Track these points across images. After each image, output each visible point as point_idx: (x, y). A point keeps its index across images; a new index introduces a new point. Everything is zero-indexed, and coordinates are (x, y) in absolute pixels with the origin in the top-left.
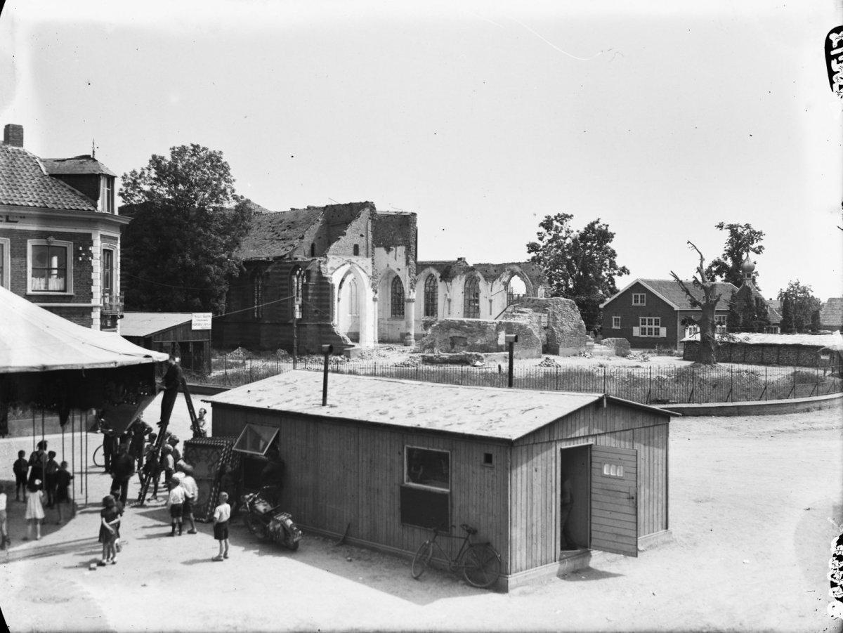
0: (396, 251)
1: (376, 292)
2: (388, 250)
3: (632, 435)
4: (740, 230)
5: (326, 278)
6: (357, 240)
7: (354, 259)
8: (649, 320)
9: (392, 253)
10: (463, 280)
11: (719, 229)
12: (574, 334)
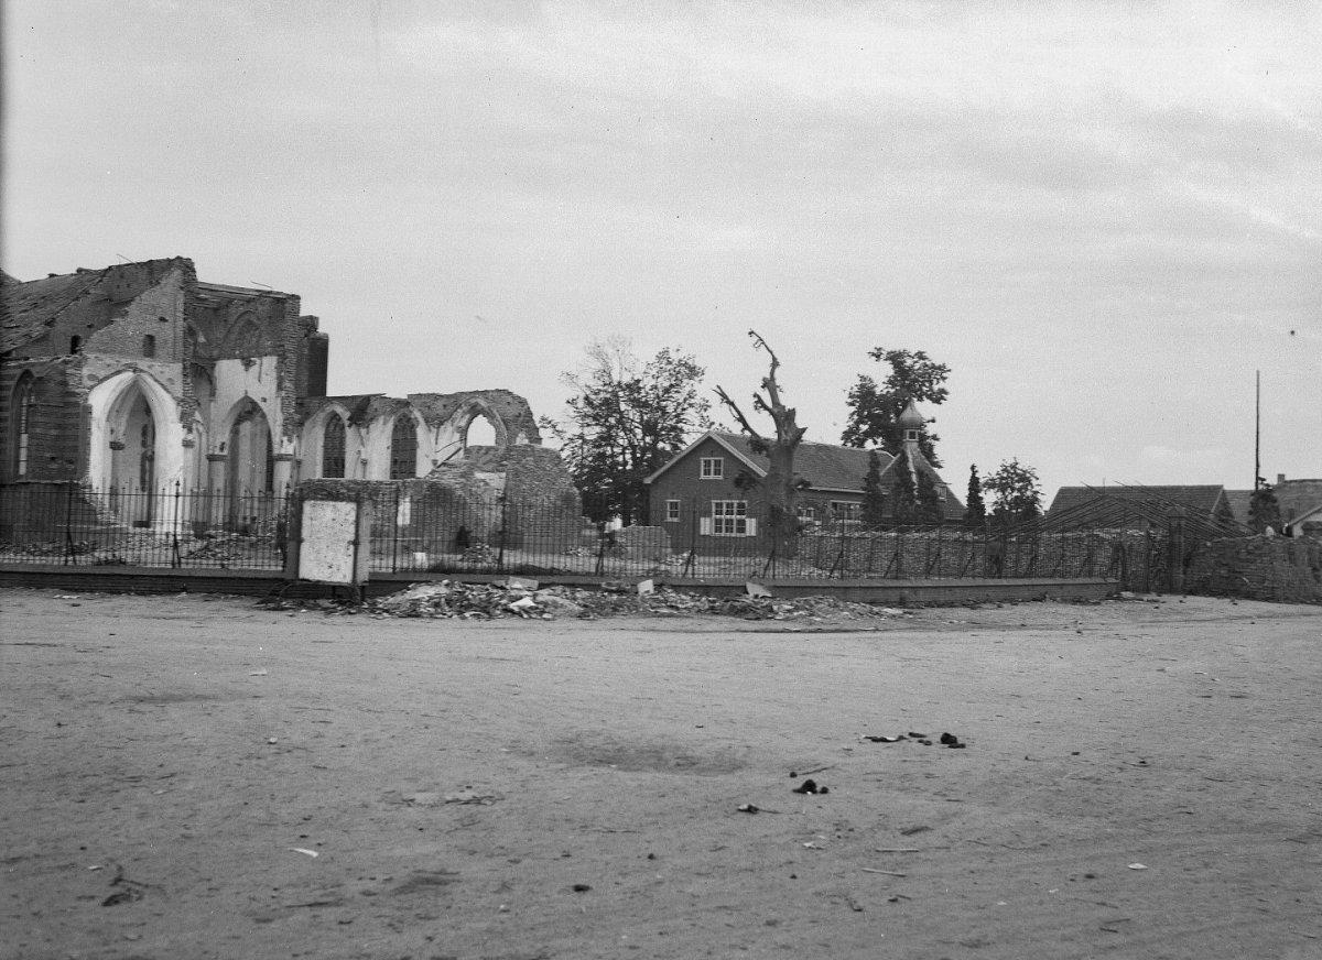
0: (261, 365)
1: (190, 431)
2: (248, 364)
3: (353, 514)
4: (909, 362)
5: (74, 394)
6: (152, 328)
7: (143, 364)
8: (728, 505)
9: (254, 369)
10: (390, 426)
11: (874, 358)
12: (557, 512)
